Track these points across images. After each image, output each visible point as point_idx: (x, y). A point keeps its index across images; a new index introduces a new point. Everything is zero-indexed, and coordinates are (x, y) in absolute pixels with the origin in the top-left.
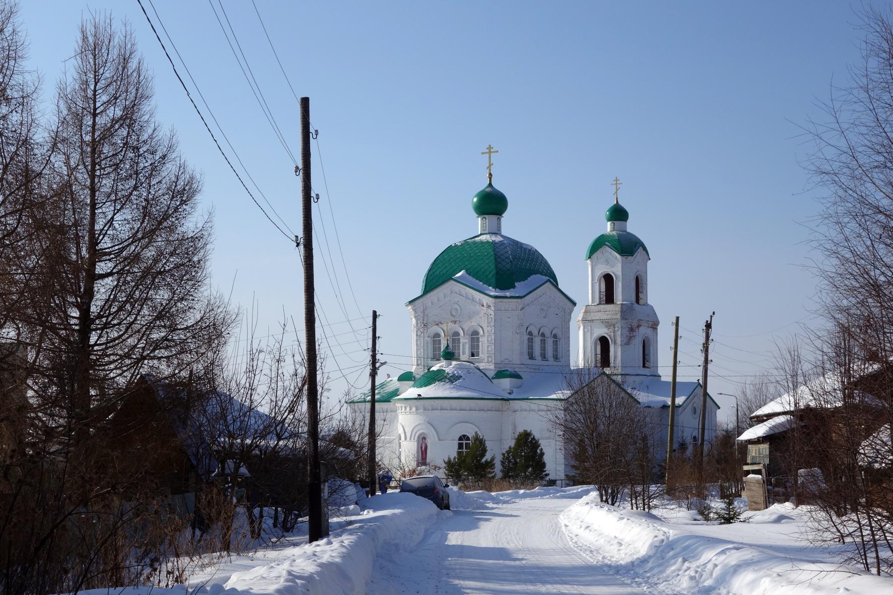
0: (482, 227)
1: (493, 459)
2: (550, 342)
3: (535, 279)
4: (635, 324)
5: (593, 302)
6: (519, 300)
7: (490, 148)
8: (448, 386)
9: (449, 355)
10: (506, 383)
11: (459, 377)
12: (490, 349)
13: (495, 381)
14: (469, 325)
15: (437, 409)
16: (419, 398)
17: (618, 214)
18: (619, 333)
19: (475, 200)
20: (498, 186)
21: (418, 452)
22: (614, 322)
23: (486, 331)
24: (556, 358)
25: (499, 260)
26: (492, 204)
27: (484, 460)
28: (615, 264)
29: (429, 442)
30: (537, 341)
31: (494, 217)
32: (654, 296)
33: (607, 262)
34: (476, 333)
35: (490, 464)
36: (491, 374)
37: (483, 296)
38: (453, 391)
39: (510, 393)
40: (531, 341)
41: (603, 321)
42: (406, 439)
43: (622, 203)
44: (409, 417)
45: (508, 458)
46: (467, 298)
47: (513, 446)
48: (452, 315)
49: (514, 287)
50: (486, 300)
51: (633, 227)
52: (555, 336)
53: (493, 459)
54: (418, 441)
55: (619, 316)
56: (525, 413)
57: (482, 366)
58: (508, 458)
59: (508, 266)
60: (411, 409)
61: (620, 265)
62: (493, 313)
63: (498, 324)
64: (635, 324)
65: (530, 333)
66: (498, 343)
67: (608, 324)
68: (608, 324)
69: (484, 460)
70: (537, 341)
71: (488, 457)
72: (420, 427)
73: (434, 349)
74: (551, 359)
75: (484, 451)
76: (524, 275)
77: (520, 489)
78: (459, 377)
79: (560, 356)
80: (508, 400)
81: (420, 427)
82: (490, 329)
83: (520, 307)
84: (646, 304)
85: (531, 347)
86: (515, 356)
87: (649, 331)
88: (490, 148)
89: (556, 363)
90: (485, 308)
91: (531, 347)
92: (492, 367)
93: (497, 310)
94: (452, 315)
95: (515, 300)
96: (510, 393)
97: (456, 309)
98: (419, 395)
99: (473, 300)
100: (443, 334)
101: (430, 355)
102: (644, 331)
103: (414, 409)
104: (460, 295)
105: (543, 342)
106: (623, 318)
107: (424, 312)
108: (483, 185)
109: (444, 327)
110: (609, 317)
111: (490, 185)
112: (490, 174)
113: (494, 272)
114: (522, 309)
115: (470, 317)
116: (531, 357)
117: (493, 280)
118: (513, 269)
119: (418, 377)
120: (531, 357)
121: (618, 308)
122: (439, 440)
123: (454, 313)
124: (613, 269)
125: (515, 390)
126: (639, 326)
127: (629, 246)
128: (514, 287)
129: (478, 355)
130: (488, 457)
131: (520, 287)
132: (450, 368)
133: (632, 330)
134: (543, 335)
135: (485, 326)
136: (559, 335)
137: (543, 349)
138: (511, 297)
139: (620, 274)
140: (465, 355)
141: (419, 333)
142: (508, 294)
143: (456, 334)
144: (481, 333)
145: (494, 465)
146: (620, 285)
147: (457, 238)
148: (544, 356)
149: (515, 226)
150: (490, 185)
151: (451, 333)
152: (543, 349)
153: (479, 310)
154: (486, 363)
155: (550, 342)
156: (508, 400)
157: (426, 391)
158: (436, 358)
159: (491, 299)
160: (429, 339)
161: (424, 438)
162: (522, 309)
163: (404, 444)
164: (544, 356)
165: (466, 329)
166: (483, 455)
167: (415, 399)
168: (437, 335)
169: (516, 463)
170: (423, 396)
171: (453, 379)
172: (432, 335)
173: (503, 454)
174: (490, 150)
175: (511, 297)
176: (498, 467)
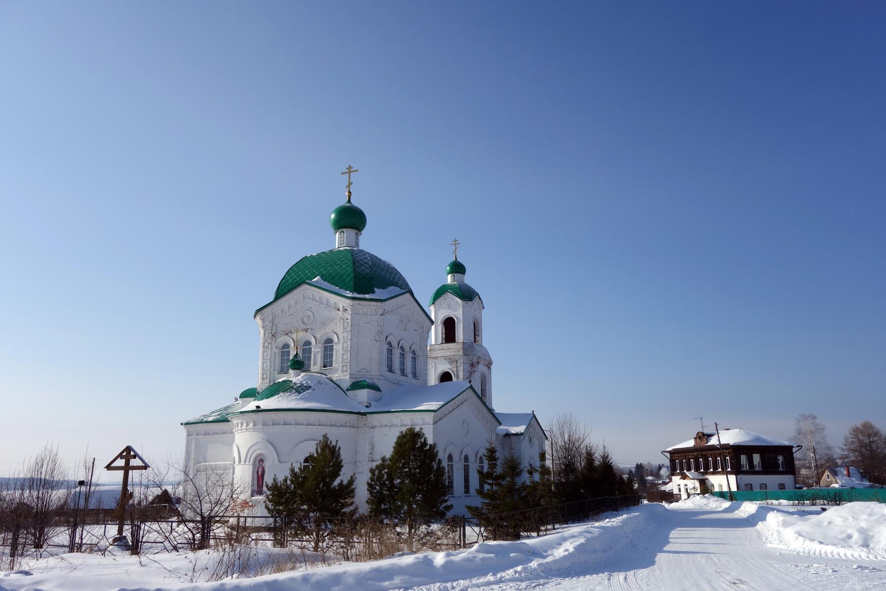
0: (340, 240)
1: (351, 481)
2: (409, 357)
3: (393, 290)
4: (475, 360)
5: (436, 341)
6: (379, 304)
7: (350, 167)
8: (294, 396)
9: (299, 365)
10: (363, 394)
11: (309, 387)
12: (345, 357)
13: (351, 393)
14: (321, 334)
15: (279, 424)
16: (258, 410)
17: (457, 268)
18: (461, 368)
19: (333, 216)
20: (355, 202)
21: (253, 479)
22: (456, 358)
23: (341, 337)
24: (415, 375)
25: (358, 264)
26: (350, 218)
27: (336, 483)
28: (455, 308)
29: (267, 465)
30: (397, 353)
31: (352, 232)
32: (489, 341)
33: (449, 307)
34: (329, 341)
35: (347, 490)
36: (345, 386)
37: (339, 298)
38: (299, 402)
39: (367, 407)
40: (390, 352)
41: (446, 358)
42: (240, 462)
43: (461, 260)
44: (246, 435)
45: (380, 477)
46: (321, 302)
47: (388, 456)
48: (303, 323)
49: (373, 292)
50: (342, 303)
51: (469, 279)
52: (414, 352)
53: (351, 481)
54: (254, 465)
55: (461, 353)
56: (385, 429)
57: (335, 377)
58: (380, 477)
59: (368, 271)
60: (247, 425)
61: (461, 309)
62: (349, 317)
63: (355, 329)
64: (475, 360)
65: (390, 344)
66: (355, 351)
67: (451, 360)
68: (451, 360)
69: (336, 483)
70: (397, 353)
71: (344, 477)
72: (257, 447)
73: (282, 361)
74: (410, 376)
75: (338, 467)
76: (384, 285)
77: (531, 561)
78: (309, 387)
79: (418, 374)
80: (364, 414)
81: (257, 447)
82: (345, 335)
83: (380, 312)
84: (481, 346)
85: (390, 359)
86: (374, 370)
87: (485, 369)
88: (350, 167)
89: (414, 381)
90: (340, 313)
91: (390, 359)
92: (348, 377)
93: (354, 314)
94: (303, 323)
95: (375, 303)
96: (367, 407)
97: (309, 316)
98: (258, 407)
99: (328, 304)
100: (292, 344)
101: (278, 367)
102: (481, 368)
103: (251, 425)
104: (314, 300)
105: (403, 356)
106: (465, 354)
107: (272, 322)
108: (343, 202)
109: (294, 336)
110: (452, 354)
111: (349, 201)
112: (350, 192)
113: (353, 275)
114: (382, 315)
115: (324, 324)
116: (390, 370)
117: (352, 283)
118: (367, 278)
119: (260, 390)
120: (390, 370)
121: (461, 346)
122: (280, 462)
123: (306, 320)
124: (455, 313)
125: (373, 403)
126: (478, 363)
127: (467, 294)
128: (373, 292)
129: (331, 365)
130: (344, 477)
131: (379, 293)
132: (295, 377)
133: (472, 365)
134: (402, 348)
135: (340, 331)
136: (418, 352)
137: (403, 363)
138: (371, 300)
139: (461, 316)
140: (316, 363)
141: (266, 344)
142: (367, 296)
143: (308, 343)
144: (336, 340)
145: (353, 491)
146: (461, 326)
147: (313, 250)
148: (403, 372)
149: (372, 242)
150: (349, 201)
151: (301, 343)
152: (403, 363)
153: (335, 314)
154: (341, 374)
155: (409, 357)
156: (364, 414)
157: (265, 404)
158: (283, 371)
159: (348, 301)
160: (277, 351)
161: (262, 461)
162: (382, 315)
163: (239, 469)
164: (403, 372)
165: (318, 336)
166: (336, 473)
167: (253, 411)
168: (286, 346)
169: (393, 486)
170: (262, 408)
171: (300, 389)
172: (280, 346)
173: (372, 471)
174: (350, 170)
175: (371, 300)
176: (362, 495)
